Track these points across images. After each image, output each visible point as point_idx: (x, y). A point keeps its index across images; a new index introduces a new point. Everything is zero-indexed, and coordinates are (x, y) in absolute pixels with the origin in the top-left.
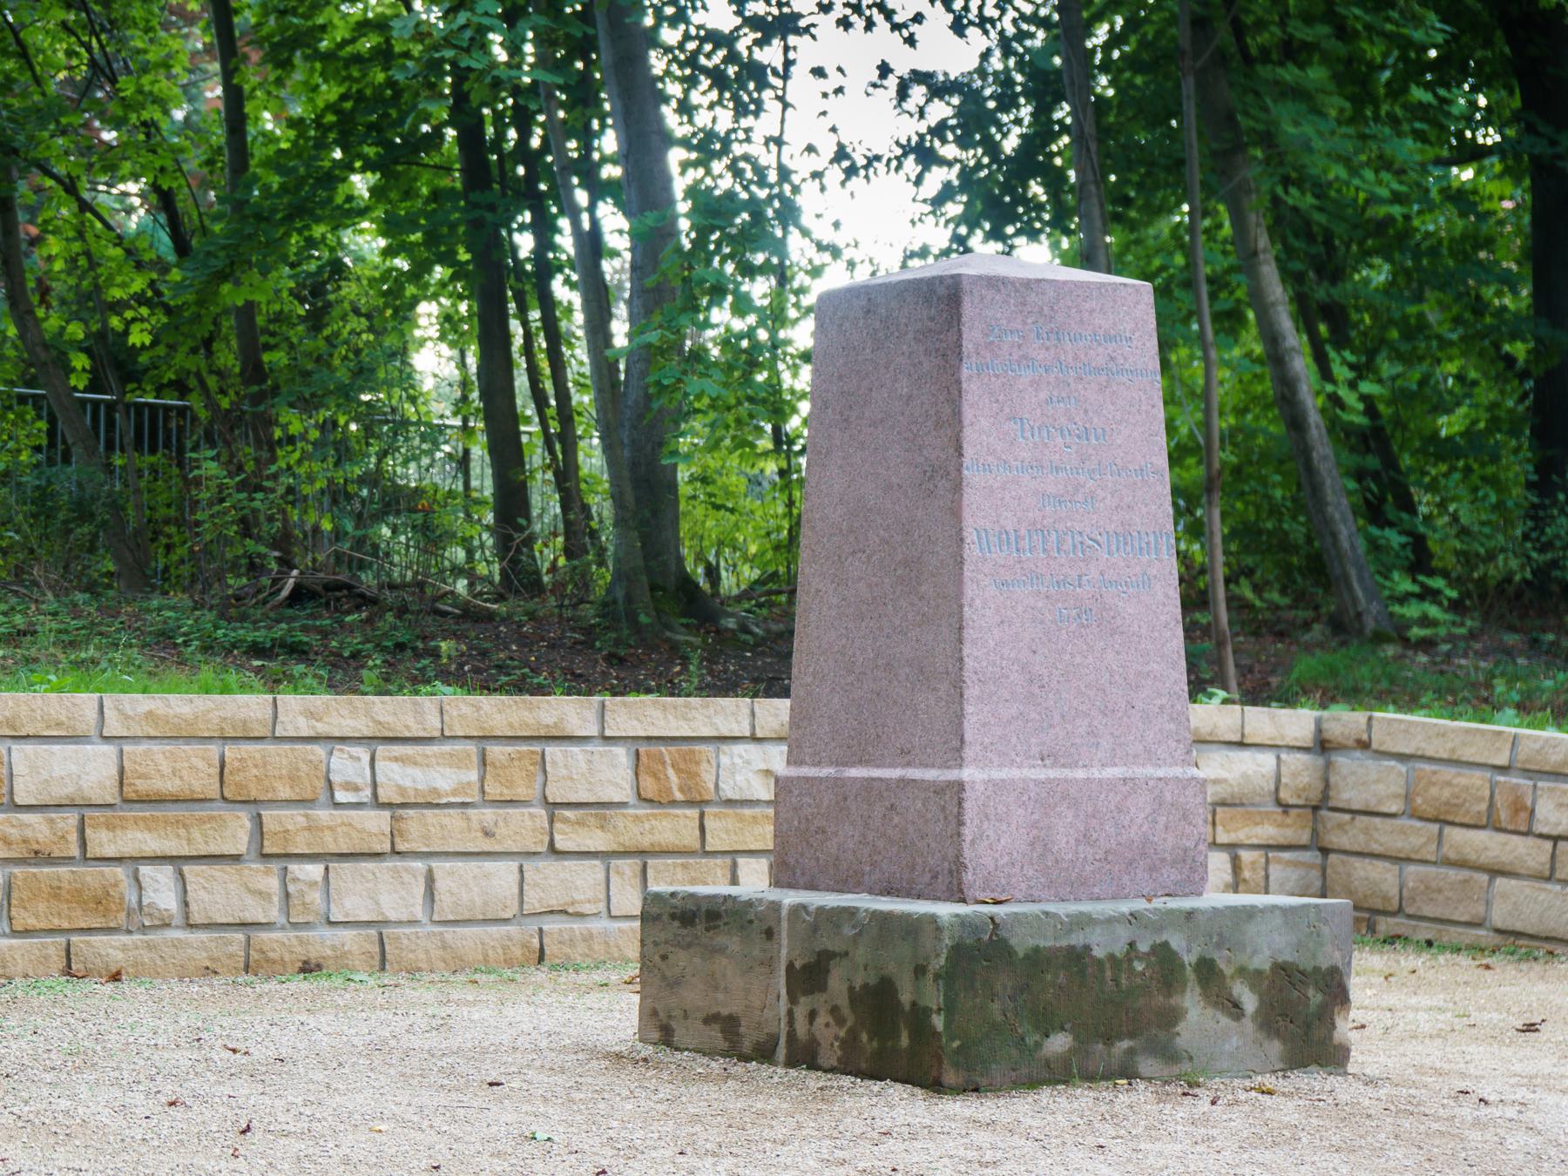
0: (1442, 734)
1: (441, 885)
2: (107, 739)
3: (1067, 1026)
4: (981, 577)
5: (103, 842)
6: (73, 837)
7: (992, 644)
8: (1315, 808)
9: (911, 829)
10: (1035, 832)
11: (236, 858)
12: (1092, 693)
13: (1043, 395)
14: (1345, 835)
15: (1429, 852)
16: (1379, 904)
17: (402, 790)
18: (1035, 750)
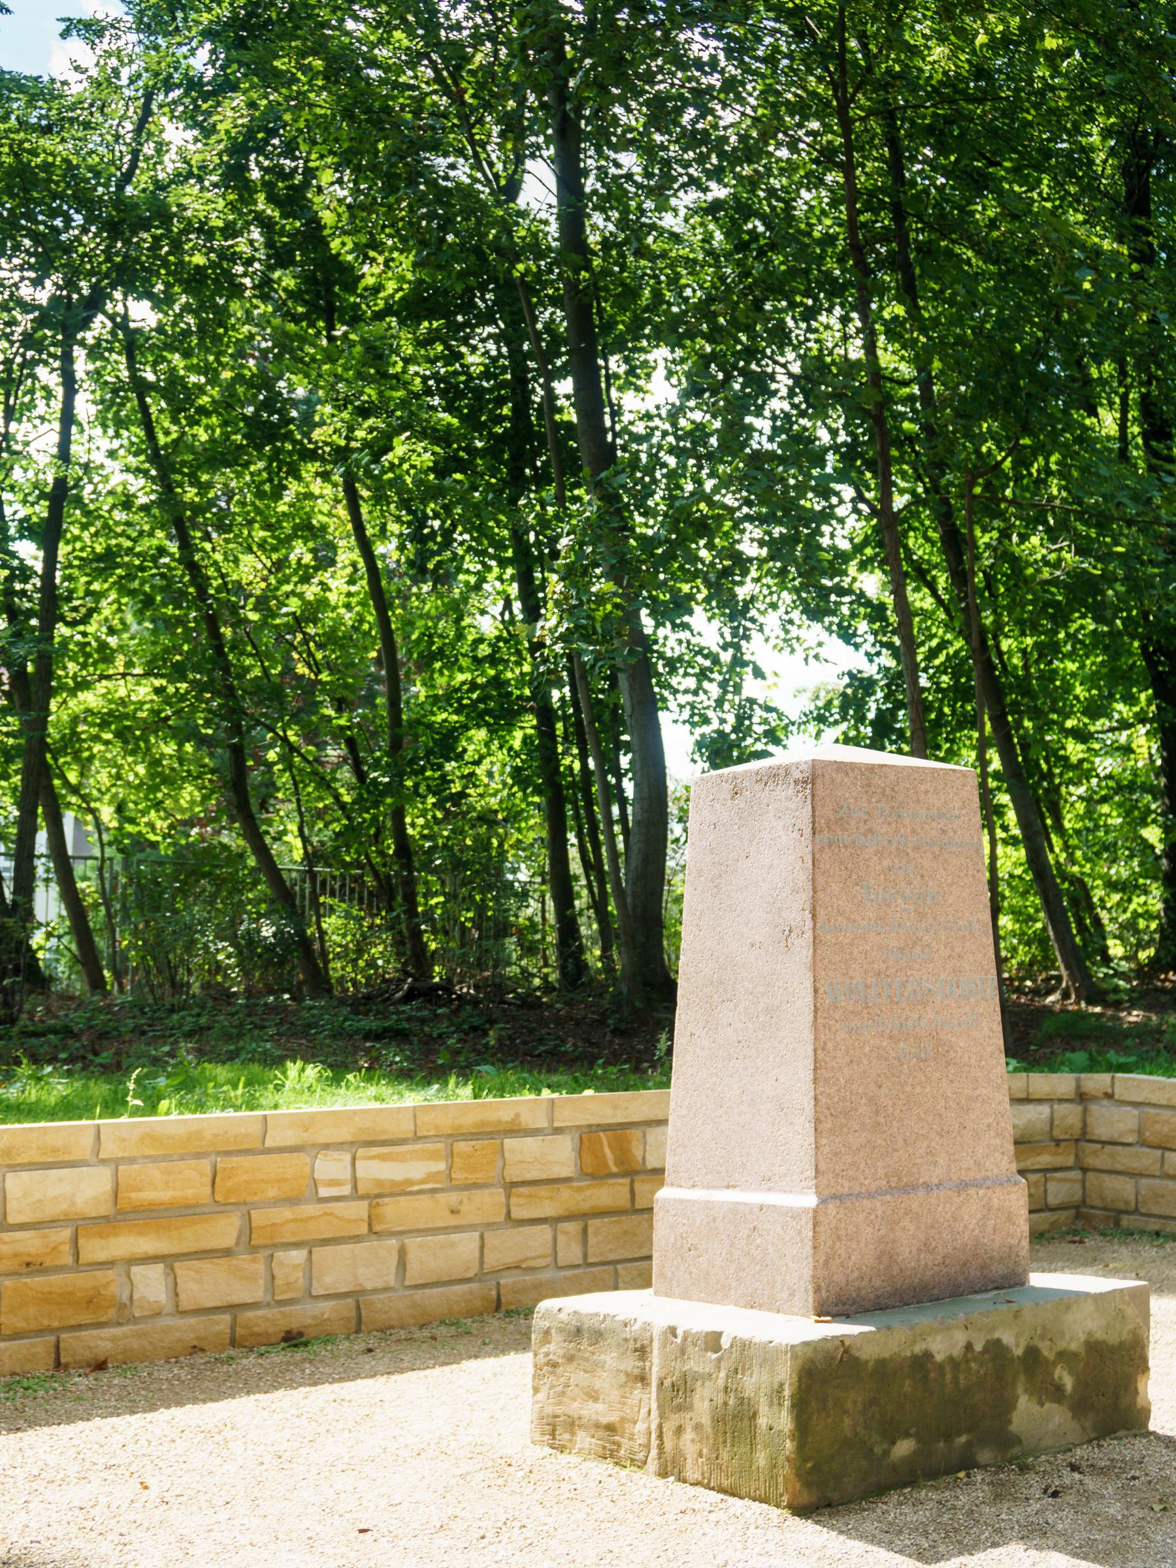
0: (1162, 1088)
1: (412, 1257)
2: (104, 1162)
3: (913, 1431)
4: (832, 1022)
5: (95, 1249)
6: (67, 1248)
7: (842, 1081)
8: (1077, 1141)
9: (771, 1249)
10: (882, 1246)
11: (227, 1253)
12: (930, 1119)
13: (886, 863)
14: (1098, 1158)
15: (1156, 1169)
16: (1122, 1206)
17: (379, 1183)
18: (881, 1172)
